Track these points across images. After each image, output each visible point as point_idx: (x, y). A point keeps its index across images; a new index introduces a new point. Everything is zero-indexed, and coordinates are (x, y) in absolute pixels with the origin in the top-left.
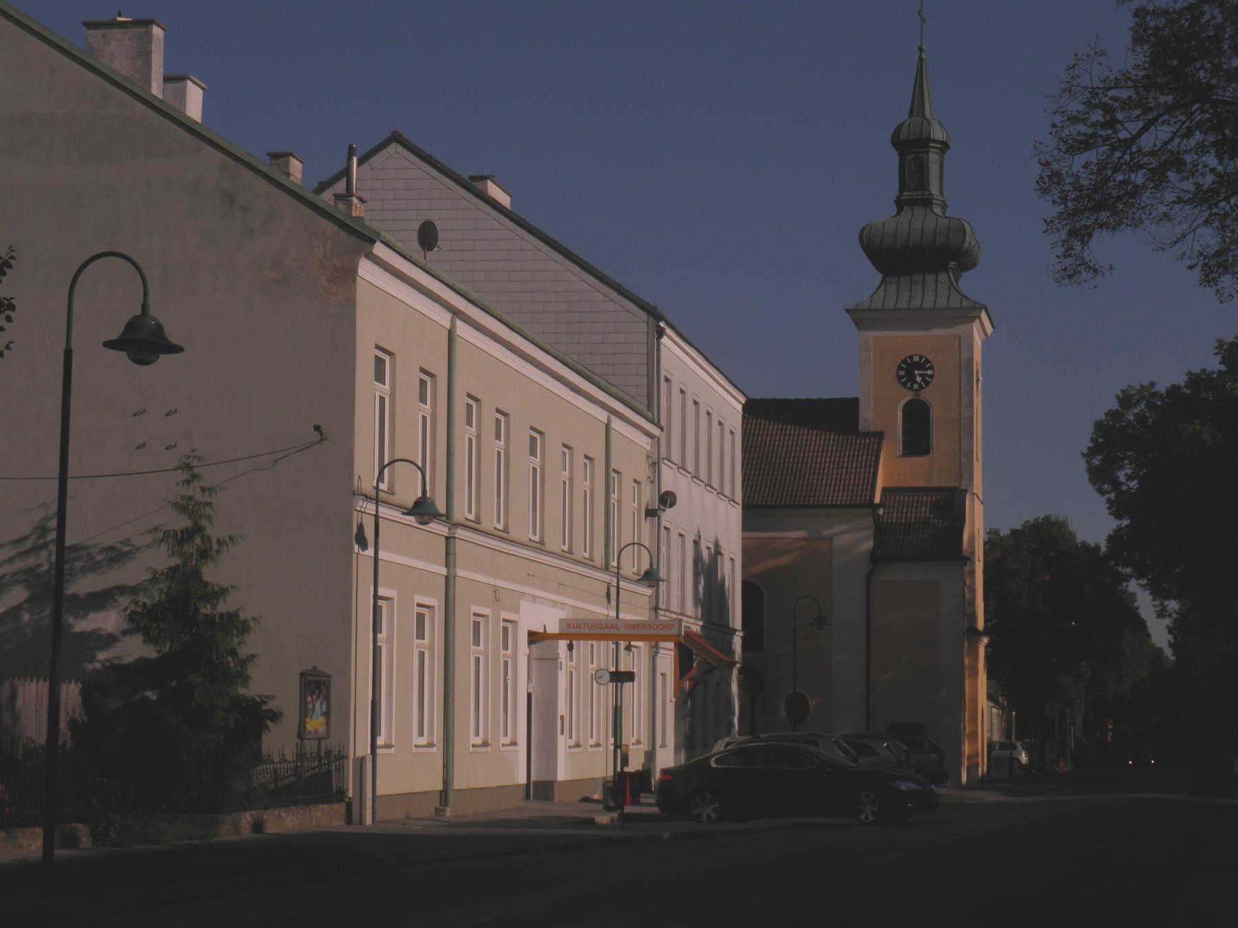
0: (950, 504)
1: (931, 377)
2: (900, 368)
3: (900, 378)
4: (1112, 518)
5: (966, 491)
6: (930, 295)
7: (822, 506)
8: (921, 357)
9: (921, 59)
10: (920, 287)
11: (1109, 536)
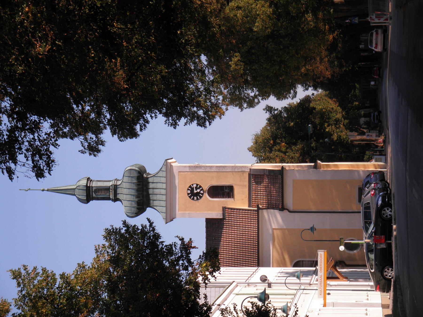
0: (256, 177)
1: (197, 185)
2: (193, 199)
3: (197, 199)
4: (269, 98)
5: (250, 169)
6: (159, 186)
7: (258, 233)
8: (188, 189)
9: (48, 190)
10: (155, 190)
11: (277, 99)
